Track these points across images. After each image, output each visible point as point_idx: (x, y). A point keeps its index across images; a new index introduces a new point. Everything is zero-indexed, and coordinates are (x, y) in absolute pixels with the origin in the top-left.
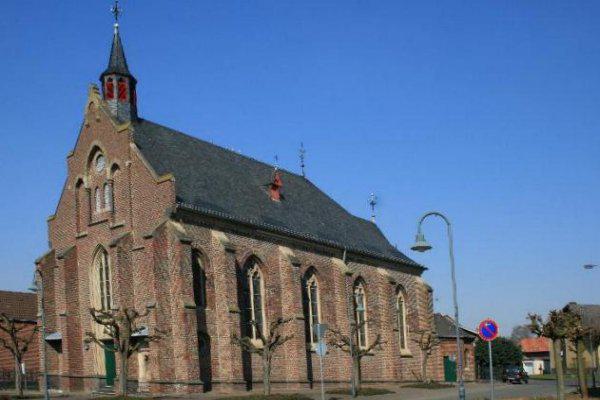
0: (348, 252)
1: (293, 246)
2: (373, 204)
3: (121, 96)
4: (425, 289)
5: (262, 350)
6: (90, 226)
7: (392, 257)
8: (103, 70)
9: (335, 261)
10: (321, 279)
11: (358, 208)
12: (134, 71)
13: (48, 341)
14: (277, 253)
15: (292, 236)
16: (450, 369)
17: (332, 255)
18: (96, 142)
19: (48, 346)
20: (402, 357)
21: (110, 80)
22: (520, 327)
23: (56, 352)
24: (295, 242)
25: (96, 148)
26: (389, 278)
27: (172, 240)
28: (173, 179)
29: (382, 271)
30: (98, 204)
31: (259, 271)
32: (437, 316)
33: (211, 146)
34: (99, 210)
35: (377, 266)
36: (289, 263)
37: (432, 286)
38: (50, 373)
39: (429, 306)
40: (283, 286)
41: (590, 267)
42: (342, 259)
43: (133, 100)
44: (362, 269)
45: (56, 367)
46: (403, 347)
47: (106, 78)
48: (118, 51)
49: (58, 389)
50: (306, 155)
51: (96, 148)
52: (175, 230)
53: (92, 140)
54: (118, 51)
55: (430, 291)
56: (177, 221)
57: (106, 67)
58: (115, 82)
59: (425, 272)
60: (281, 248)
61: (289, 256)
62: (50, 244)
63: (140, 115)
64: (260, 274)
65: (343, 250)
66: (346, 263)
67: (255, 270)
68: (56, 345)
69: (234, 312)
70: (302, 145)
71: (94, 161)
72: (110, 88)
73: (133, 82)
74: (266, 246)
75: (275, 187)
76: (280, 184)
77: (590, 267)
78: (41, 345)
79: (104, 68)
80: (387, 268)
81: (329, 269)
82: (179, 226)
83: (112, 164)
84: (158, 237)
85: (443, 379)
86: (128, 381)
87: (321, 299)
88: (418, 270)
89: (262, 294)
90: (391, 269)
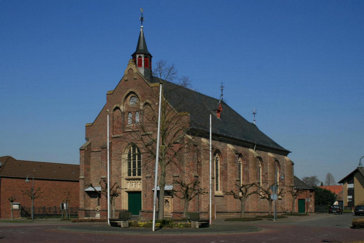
0: (257, 145)
1: (233, 144)
2: (254, 114)
4: (290, 163)
5: (242, 197)
6: (124, 132)
9: (251, 150)
10: (243, 160)
11: (250, 119)
12: (150, 51)
13: (86, 191)
15: (232, 138)
16: (302, 204)
17: (249, 147)
19: (86, 194)
20: (216, 196)
22: (308, 178)
23: (89, 197)
24: (235, 142)
26: (275, 158)
28: (189, 115)
29: (270, 154)
31: (218, 157)
32: (295, 177)
35: (267, 151)
36: (234, 153)
37: (294, 162)
38: (86, 209)
39: (291, 171)
40: (229, 164)
41: (142, 18)
42: (253, 149)
44: (262, 154)
45: (89, 206)
46: (217, 189)
47: (137, 56)
48: (141, 40)
49: (90, 217)
54: (141, 40)
55: (293, 164)
56: (189, 134)
59: (290, 154)
60: (228, 145)
61: (233, 149)
62: (87, 139)
64: (219, 159)
65: (254, 145)
66: (255, 151)
67: (216, 156)
68: (94, 194)
71: (129, 97)
72: (140, 61)
73: (151, 57)
74: (223, 144)
75: (219, 111)
76: (221, 110)
77: (142, 18)
78: (81, 194)
80: (272, 152)
81: (247, 154)
82: (190, 137)
85: (298, 211)
87: (243, 170)
88: (286, 153)
89: (219, 168)
90: (274, 153)
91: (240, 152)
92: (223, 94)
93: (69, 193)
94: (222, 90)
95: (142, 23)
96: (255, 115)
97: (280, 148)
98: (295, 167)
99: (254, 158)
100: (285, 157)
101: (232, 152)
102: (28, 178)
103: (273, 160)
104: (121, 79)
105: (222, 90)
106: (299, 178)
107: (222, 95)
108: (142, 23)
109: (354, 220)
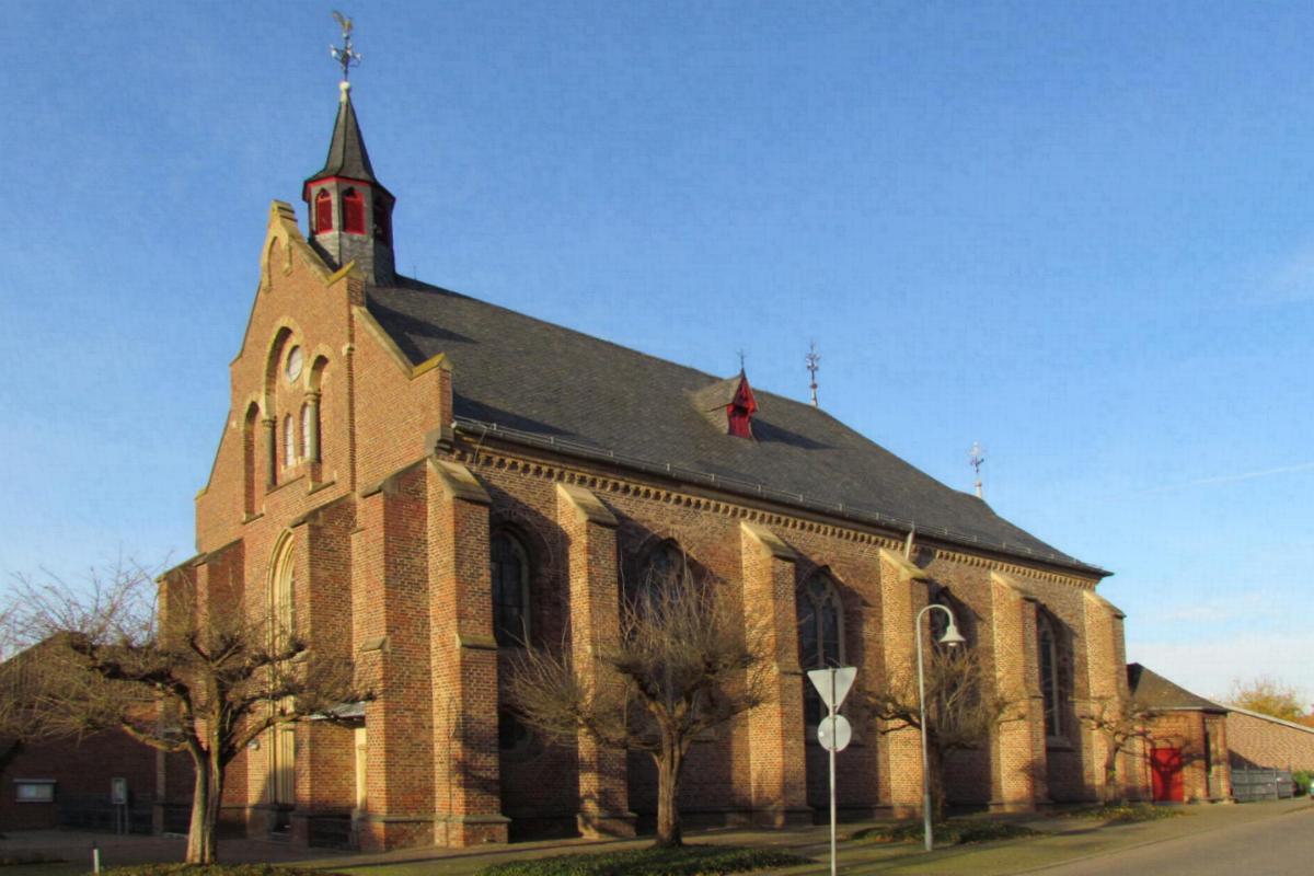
3: (350, 223)
4: (1105, 615)
7: (1029, 551)
8: (310, 174)
11: (959, 480)
14: (735, 537)
18: (284, 322)
21: (324, 193)
25: (285, 333)
27: (439, 500)
30: (291, 450)
33: (672, 365)
34: (292, 461)
36: (766, 554)
43: (384, 237)
47: (315, 190)
48: (350, 134)
50: (821, 365)
51: (285, 333)
52: (449, 477)
53: (279, 315)
54: (350, 134)
57: (322, 167)
58: (334, 199)
59: (1105, 580)
63: (403, 268)
65: (905, 534)
69: (1035, 697)
70: (812, 347)
72: (324, 210)
73: (384, 203)
79: (317, 165)
83: (314, 358)
84: (404, 490)
86: (1234, 784)
88: (1095, 575)
91: (821, 560)
92: (816, 381)
93: (393, 776)
94: (813, 369)
95: (346, 72)
96: (980, 467)
97: (1052, 557)
98: (1128, 625)
99: (900, 583)
100: (1086, 594)
101: (758, 552)
102: (1222, 800)
103: (1012, 598)
104: (248, 318)
105: (813, 369)
106: (1169, 679)
107: (814, 386)
108: (346, 72)
109: (932, 575)
